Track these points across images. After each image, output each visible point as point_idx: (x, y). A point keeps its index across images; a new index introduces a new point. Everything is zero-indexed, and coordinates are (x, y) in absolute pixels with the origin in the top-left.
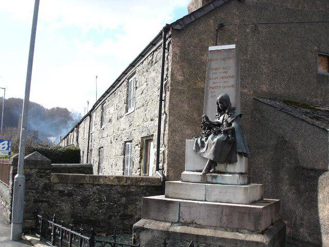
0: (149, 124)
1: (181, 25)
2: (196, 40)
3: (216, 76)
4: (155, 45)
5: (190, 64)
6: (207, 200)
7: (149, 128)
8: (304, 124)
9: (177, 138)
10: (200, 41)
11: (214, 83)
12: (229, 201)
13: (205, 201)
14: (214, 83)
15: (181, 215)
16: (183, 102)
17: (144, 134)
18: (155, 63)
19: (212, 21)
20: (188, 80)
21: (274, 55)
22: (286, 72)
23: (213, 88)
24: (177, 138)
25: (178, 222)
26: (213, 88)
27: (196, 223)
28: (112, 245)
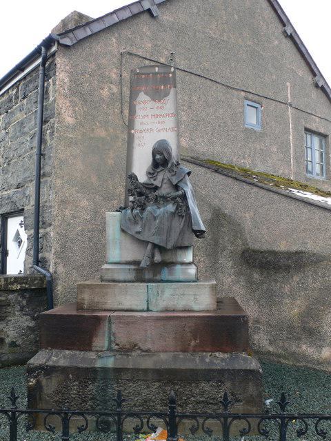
0: (15, 193)
1: (71, 39)
2: (93, 66)
3: (145, 113)
4: (23, 70)
5: (86, 102)
6: (151, 308)
7: (14, 199)
8: (255, 189)
9: (67, 212)
10: (99, 66)
11: (142, 123)
12: (187, 308)
13: (148, 310)
14: (142, 123)
15: (112, 338)
16: (75, 157)
17: (303, 132)
18: (24, 98)
19: (114, 40)
20: (81, 124)
21: (194, 98)
22: (209, 123)
23: (141, 132)
24: (67, 212)
25: (110, 349)
26: (141, 132)
27: (139, 349)
28: (8, 416)
